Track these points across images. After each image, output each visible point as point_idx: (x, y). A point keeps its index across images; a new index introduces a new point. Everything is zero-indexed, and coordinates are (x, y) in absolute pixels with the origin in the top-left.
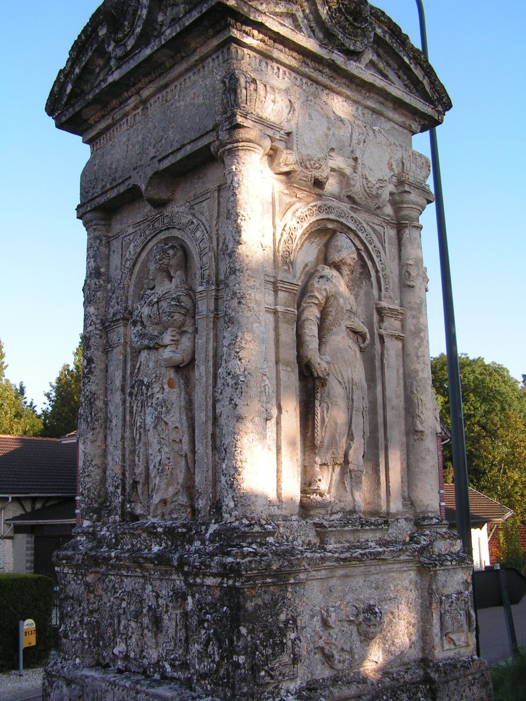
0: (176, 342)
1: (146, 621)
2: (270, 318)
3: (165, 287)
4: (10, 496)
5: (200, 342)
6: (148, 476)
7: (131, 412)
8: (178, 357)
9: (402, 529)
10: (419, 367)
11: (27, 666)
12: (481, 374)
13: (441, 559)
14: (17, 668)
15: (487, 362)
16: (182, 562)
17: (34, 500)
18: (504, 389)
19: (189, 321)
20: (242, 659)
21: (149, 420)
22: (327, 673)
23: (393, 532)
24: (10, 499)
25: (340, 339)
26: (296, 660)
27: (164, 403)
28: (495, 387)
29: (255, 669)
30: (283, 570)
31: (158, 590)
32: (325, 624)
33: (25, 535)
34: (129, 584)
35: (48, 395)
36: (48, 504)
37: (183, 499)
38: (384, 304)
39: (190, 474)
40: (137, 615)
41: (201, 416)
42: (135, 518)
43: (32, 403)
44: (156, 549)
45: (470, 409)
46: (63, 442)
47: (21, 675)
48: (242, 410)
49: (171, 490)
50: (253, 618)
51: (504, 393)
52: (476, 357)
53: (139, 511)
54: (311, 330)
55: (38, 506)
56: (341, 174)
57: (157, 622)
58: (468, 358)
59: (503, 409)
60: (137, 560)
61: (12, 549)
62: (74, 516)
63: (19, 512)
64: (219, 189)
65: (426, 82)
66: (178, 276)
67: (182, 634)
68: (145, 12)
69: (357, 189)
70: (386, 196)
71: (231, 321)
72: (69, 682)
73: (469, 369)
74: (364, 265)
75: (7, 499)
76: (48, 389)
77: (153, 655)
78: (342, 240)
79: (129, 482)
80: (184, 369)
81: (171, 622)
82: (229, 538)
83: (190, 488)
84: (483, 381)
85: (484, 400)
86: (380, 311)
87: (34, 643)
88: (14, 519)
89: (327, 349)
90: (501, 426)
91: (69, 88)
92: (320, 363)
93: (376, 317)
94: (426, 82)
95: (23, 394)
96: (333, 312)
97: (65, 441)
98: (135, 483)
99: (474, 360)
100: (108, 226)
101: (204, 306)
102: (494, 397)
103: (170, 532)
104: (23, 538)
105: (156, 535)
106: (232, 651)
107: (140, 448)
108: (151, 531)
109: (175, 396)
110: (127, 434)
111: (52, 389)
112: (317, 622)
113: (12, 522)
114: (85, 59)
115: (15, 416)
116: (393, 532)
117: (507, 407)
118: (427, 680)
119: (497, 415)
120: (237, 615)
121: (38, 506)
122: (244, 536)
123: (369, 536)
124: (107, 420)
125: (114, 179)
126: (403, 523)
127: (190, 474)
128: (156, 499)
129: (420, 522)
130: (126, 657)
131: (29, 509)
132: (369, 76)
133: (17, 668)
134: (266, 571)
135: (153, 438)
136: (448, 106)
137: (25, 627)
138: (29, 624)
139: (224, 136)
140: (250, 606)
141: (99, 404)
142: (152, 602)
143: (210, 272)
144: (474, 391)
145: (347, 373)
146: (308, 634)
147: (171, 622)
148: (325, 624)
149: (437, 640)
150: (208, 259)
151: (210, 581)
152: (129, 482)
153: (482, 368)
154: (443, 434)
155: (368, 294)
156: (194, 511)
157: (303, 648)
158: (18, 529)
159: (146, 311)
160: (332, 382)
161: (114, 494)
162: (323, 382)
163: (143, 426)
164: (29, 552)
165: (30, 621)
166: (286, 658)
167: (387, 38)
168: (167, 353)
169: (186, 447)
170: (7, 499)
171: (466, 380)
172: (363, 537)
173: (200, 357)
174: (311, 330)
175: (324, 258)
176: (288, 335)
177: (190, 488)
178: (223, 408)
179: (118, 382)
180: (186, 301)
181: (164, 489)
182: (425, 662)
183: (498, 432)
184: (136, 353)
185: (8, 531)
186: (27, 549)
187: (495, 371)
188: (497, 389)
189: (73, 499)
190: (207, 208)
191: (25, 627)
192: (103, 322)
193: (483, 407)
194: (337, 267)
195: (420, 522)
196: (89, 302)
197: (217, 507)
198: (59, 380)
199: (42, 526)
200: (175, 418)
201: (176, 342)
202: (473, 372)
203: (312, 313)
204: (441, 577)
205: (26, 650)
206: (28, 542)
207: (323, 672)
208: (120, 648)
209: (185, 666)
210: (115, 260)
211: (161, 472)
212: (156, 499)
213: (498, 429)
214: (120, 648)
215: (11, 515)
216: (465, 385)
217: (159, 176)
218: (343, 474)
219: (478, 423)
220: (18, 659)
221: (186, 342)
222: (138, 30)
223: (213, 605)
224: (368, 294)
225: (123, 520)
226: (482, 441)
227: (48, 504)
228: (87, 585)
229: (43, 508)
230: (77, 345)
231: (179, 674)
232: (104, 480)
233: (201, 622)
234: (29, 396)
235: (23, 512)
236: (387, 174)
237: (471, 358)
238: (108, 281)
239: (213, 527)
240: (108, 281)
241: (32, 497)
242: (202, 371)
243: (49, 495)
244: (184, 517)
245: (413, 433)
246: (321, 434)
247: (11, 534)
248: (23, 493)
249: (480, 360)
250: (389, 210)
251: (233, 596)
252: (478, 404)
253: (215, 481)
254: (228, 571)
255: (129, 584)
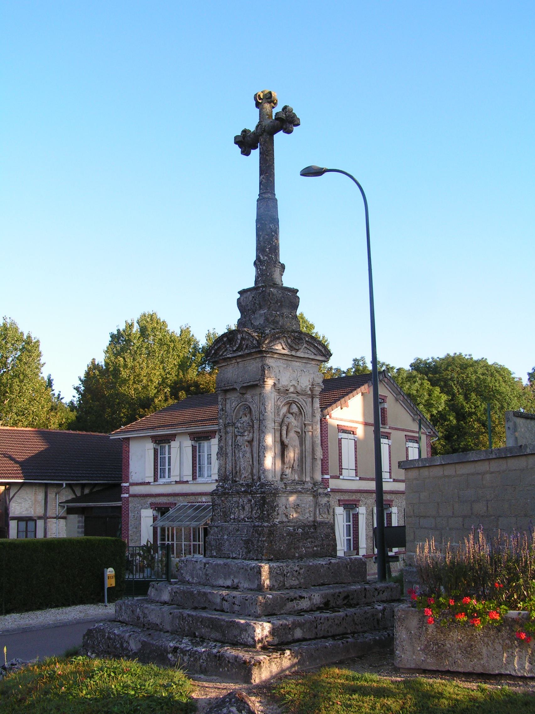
0: (248, 435)
1: (240, 508)
2: (273, 430)
3: (244, 419)
4: (64, 483)
5: (255, 435)
6: (240, 470)
7: (235, 452)
8: (249, 439)
9: (310, 486)
10: (316, 440)
11: (109, 601)
12: (483, 374)
13: (320, 494)
14: (103, 602)
15: (490, 362)
16: (251, 491)
17: (83, 486)
18: (504, 388)
19: (252, 430)
20: (265, 512)
21: (241, 455)
22: (286, 520)
23: (306, 486)
24: (64, 485)
25: (292, 434)
26: (278, 514)
27: (245, 451)
28: (495, 387)
29: (268, 515)
30: (275, 493)
31: (243, 500)
32: (286, 508)
33: (77, 516)
34: (235, 499)
35: (77, 389)
36: (95, 490)
37: (250, 476)
38: (306, 422)
39: (252, 470)
40: (238, 507)
41: (255, 455)
42: (236, 482)
43: (59, 395)
44: (243, 489)
45: (471, 407)
46: (111, 438)
47: (106, 606)
48: (266, 455)
49: (247, 474)
50: (268, 503)
51: (503, 393)
52: (480, 358)
53: (237, 480)
54: (284, 432)
55: (87, 491)
56: (294, 385)
57: (243, 508)
58: (471, 359)
59: (502, 408)
60: (238, 493)
61: (65, 528)
62: (120, 499)
63: (71, 496)
64: (260, 394)
65: (323, 350)
66: (248, 415)
67: (250, 510)
68: (239, 341)
69: (299, 389)
70: (308, 389)
71: (263, 432)
72: (217, 527)
73: (471, 369)
74: (301, 411)
75: (62, 485)
76: (78, 383)
77: (242, 517)
78: (294, 406)
79: (234, 472)
80: (250, 442)
81: (247, 508)
82: (262, 485)
83: (252, 473)
84: (484, 380)
85: (485, 399)
86: (305, 424)
87: (114, 585)
88: (67, 502)
89: (288, 437)
90: (500, 423)
91: (213, 352)
92: (286, 441)
93: (304, 426)
94: (323, 350)
95: (51, 386)
96: (290, 426)
97: (114, 436)
98: (237, 472)
99: (476, 362)
100: (225, 395)
101: (256, 426)
102: (494, 396)
103: (247, 485)
104: (74, 518)
105: (243, 486)
106: (263, 511)
107: (238, 463)
108: (242, 485)
109: (248, 449)
110: (233, 458)
111: (81, 383)
112: (284, 507)
113: (66, 505)
114: (219, 345)
115: (51, 410)
116: (306, 486)
117: (505, 405)
118: (314, 525)
119: (496, 413)
120: (264, 502)
121: (87, 491)
122: (266, 485)
123: (299, 486)
124: (226, 454)
125: (228, 383)
126: (309, 484)
127: (252, 470)
128: (243, 476)
129: (315, 484)
130: (234, 519)
131: (79, 494)
132: (302, 355)
133: (103, 602)
134: (271, 493)
135: (242, 460)
136: (331, 355)
137: (108, 573)
138: (110, 571)
139: (261, 383)
140: (267, 501)
141: (224, 449)
142: (242, 503)
143: (257, 417)
144: (476, 391)
145: (294, 444)
146: (282, 510)
147: (247, 508)
148: (286, 508)
149: (318, 515)
150: (257, 413)
151: (258, 495)
152: (234, 472)
153: (485, 368)
154: (432, 433)
155: (302, 419)
156: (253, 480)
157: (280, 512)
158: (70, 511)
159: (239, 425)
160: (289, 446)
161: (229, 475)
162: (287, 447)
163: (239, 457)
164: (80, 530)
165: (111, 569)
166: (276, 513)
167: (310, 340)
168: (246, 438)
169: (251, 463)
170: (62, 485)
171: (468, 380)
172: (297, 487)
173: (255, 439)
174: (284, 432)
175: (289, 411)
176: (278, 435)
177: (252, 473)
178: (261, 454)
179: (230, 444)
180: (251, 424)
181: (245, 474)
182: (314, 521)
183: (496, 429)
184: (236, 436)
185: (62, 512)
186: (78, 527)
187: (497, 371)
188: (497, 388)
189: (119, 485)
190: (256, 398)
191: (108, 573)
192: (225, 425)
193: (483, 406)
194: (292, 414)
195: (315, 484)
196: (327, 536)
197: (259, 478)
198: (87, 374)
199: (92, 508)
200: (248, 455)
201: (248, 435)
202: (476, 372)
203: (284, 428)
204: (320, 499)
205: (109, 588)
206: (79, 522)
207: (285, 519)
208: (232, 516)
209: (251, 518)
210: (228, 406)
211: (244, 469)
212: (243, 476)
213: (497, 426)
214: (232, 516)
215: (64, 499)
216: (467, 384)
217: (243, 387)
218: (292, 470)
219: (478, 420)
220: (104, 596)
221: (251, 435)
222: (237, 346)
223: (259, 501)
224: (302, 419)
225: (232, 482)
226: (481, 437)
227: (95, 490)
228: (222, 500)
229: (91, 493)
230: (107, 343)
231: (250, 520)
232: (226, 471)
233: (256, 505)
234: (57, 388)
235: (74, 497)
236: (308, 383)
237: (475, 358)
238: (226, 412)
239: (258, 483)
240: (226, 412)
241: (82, 484)
242: (255, 443)
243: (96, 482)
244: (250, 481)
245: (314, 459)
246: (286, 460)
247: (65, 515)
248: (72, 480)
249: (483, 361)
250: (309, 392)
251: (263, 499)
252: (479, 403)
253: (259, 472)
254: (262, 493)
255: (235, 499)
